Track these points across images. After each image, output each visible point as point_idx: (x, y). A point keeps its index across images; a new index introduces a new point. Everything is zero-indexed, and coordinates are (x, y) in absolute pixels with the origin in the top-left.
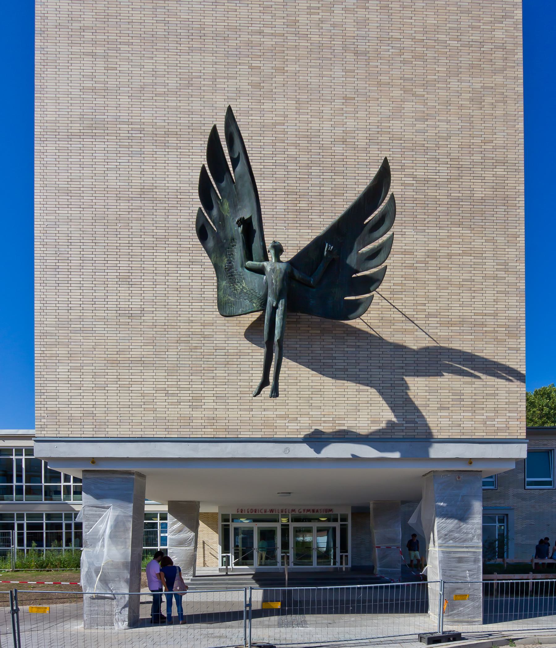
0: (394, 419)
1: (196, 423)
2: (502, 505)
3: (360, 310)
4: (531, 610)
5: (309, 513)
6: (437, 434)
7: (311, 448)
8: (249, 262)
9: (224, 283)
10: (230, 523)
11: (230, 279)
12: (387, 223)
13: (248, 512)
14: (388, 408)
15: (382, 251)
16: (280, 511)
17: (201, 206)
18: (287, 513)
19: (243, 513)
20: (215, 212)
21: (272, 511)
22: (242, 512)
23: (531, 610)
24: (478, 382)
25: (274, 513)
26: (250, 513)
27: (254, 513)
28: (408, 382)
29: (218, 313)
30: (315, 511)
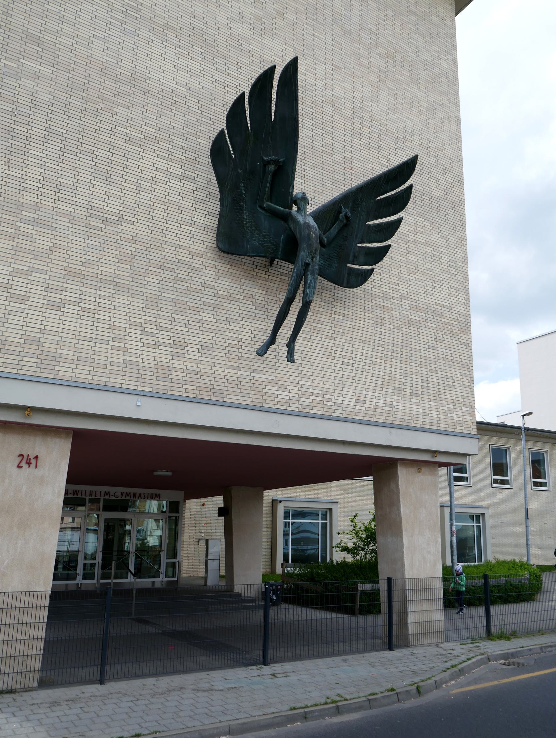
1: (177, 375)
2: (325, 497)
16: (88, 493)
25: (79, 496)
30: (137, 495)
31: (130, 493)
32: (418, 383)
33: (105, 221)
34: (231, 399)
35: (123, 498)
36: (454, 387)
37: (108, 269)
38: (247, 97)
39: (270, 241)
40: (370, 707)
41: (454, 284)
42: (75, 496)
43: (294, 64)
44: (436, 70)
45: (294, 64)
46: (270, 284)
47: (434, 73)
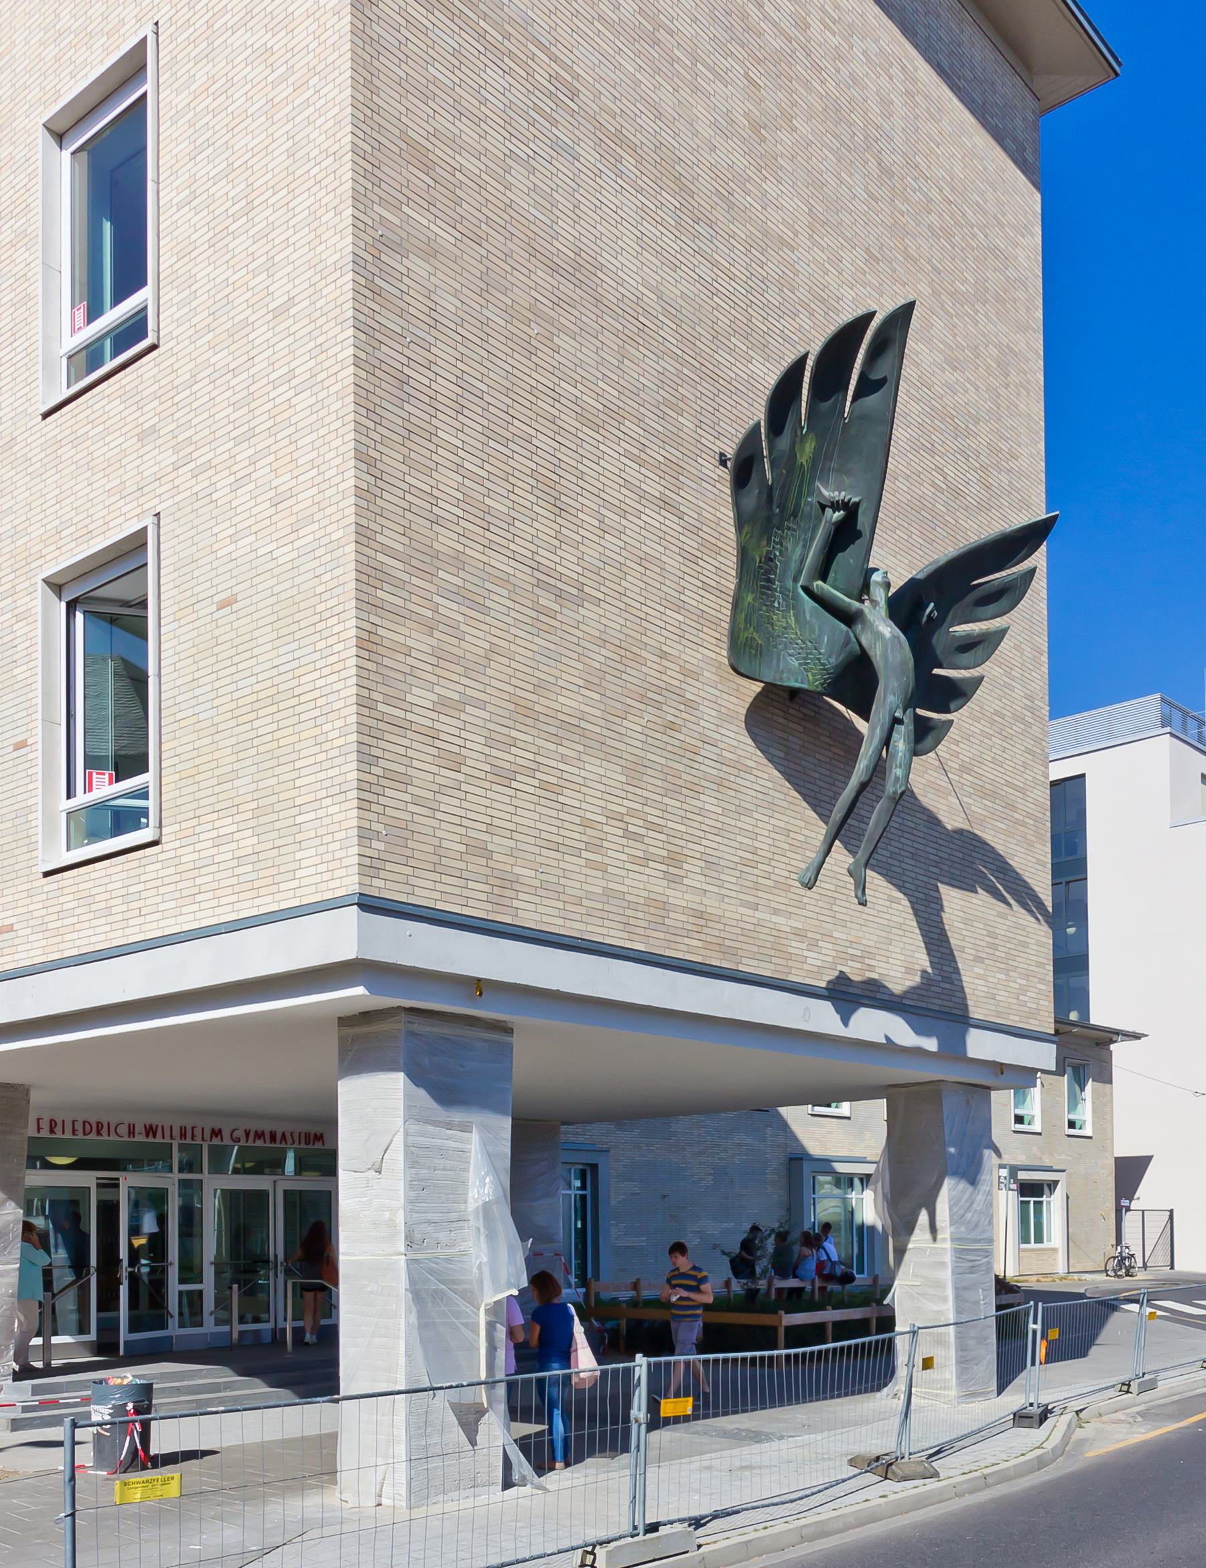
0: (930, 970)
1: (677, 919)
2: (580, 1139)
3: (912, 737)
4: (853, 1385)
5: (259, 1143)
6: (976, 1013)
7: (838, 1012)
8: (820, 583)
9: (749, 598)
10: (205, 1176)
11: (763, 593)
12: (1003, 602)
13: (74, 1132)
14: (922, 945)
15: (981, 646)
16: (176, 1133)
17: (763, 417)
18: (199, 1141)
19: (59, 1135)
20: (784, 442)
21: (150, 1130)
22: (52, 1131)
23: (853, 1385)
24: (1036, 926)
25: (159, 1139)
26: (80, 1136)
27: (93, 1136)
28: (943, 897)
29: (726, 661)
30: (279, 1137)
31: (263, 1133)
32: (401, 805)
33: (559, 595)
34: (748, 966)
35: (250, 1143)
36: (1025, 945)
37: (569, 702)
38: (810, 363)
39: (819, 659)
40: (987, 1486)
41: (1029, 743)
42: (151, 1139)
43: (903, 315)
44: (1011, 272)
45: (903, 315)
46: (791, 738)
47: (1007, 278)
